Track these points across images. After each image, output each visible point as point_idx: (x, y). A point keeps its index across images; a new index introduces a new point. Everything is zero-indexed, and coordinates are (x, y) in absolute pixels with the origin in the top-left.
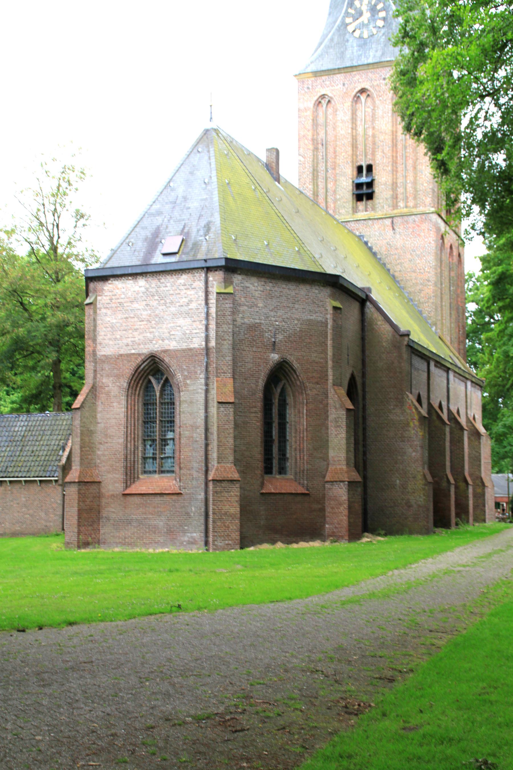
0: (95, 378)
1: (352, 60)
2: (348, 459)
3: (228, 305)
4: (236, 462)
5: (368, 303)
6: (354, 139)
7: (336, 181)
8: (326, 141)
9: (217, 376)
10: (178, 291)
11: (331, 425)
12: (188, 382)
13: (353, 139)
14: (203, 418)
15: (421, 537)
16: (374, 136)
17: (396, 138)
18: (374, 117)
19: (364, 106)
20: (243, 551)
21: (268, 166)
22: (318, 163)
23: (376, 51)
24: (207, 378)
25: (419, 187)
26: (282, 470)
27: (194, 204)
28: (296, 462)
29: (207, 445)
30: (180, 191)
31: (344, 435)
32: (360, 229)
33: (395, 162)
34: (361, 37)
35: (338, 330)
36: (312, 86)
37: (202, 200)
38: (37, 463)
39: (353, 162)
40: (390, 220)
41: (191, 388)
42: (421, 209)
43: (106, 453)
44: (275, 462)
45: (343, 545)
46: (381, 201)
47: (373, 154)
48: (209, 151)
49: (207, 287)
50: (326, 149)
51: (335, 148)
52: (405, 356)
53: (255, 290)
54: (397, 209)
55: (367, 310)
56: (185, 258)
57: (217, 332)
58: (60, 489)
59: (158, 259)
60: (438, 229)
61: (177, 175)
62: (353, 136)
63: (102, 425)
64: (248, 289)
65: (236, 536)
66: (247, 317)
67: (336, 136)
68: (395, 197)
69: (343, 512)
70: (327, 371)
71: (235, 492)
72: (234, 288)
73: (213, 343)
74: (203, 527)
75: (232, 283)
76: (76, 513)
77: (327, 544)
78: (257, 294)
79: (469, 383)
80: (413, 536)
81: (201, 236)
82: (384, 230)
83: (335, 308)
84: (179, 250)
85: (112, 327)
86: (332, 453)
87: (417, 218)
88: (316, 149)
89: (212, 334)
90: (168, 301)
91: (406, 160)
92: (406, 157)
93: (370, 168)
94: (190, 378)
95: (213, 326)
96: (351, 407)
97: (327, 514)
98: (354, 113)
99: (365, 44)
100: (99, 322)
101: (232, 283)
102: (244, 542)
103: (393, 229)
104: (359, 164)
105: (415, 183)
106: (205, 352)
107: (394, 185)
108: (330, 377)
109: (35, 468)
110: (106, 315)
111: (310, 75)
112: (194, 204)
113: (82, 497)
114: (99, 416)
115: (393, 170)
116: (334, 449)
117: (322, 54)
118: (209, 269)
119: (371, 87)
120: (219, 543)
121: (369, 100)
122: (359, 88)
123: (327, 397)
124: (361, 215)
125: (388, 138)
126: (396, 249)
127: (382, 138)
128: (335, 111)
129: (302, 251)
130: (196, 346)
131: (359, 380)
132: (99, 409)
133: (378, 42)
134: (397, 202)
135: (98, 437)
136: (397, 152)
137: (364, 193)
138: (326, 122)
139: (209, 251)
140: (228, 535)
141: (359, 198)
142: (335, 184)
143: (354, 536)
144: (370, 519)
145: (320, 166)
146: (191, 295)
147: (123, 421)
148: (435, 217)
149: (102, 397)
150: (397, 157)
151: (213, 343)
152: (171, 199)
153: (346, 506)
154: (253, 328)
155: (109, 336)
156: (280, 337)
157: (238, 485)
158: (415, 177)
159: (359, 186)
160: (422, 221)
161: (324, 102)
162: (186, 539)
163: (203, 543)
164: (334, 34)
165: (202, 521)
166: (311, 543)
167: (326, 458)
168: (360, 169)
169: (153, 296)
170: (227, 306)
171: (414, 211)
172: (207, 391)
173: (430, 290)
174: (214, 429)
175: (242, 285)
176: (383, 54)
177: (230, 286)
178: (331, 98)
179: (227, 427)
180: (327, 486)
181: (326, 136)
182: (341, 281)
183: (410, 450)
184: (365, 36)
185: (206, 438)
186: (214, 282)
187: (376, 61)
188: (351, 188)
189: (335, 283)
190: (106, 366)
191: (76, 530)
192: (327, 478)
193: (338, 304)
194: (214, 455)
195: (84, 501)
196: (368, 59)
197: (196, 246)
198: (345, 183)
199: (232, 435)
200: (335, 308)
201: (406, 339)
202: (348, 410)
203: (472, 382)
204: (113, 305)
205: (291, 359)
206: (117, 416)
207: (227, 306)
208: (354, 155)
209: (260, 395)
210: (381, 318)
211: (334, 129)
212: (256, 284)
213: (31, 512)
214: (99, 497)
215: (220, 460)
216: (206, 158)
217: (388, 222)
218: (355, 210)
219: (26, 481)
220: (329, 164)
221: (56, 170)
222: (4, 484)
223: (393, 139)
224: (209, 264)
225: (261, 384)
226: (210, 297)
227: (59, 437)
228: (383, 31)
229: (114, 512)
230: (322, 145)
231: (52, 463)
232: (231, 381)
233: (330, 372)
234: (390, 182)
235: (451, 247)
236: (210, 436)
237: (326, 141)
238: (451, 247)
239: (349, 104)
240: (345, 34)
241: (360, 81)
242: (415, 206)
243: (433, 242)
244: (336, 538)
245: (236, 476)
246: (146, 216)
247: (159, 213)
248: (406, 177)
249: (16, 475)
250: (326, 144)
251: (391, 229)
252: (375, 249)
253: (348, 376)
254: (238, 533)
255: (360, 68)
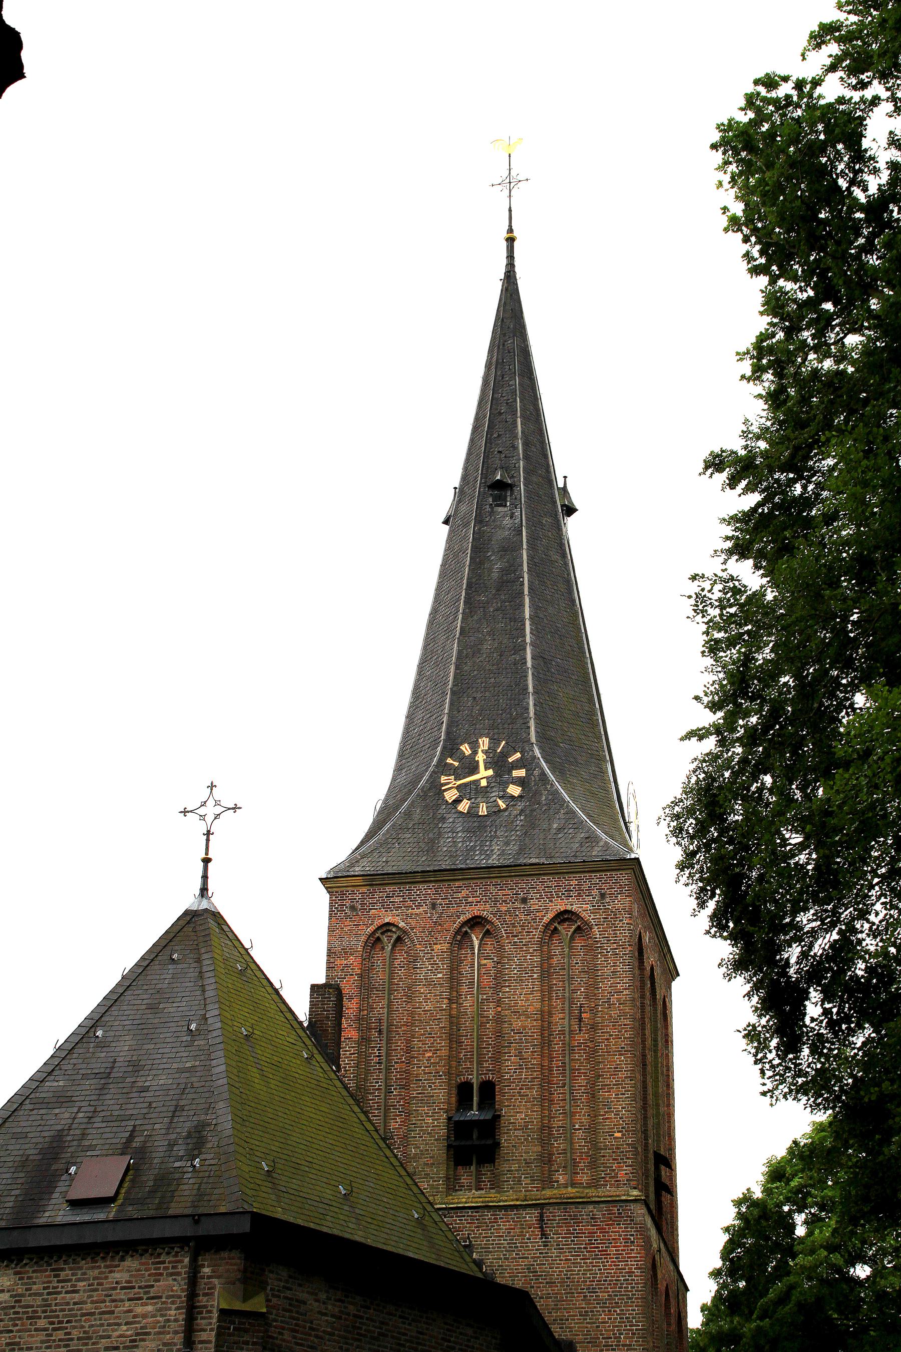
6: (454, 1021)
7: (409, 1114)
8: (390, 1025)
10: (108, 1305)
13: (451, 1023)
16: (499, 1020)
17: (549, 1028)
19: (478, 954)
23: (507, 844)
25: (603, 1140)
27: (159, 1080)
30: (124, 1049)
33: (546, 1081)
36: (363, 904)
37: (180, 1071)
39: (449, 1073)
40: (536, 1212)
42: (609, 1191)
46: (515, 1167)
47: (497, 1058)
48: (199, 961)
49: (192, 1295)
51: (408, 1041)
53: (320, 1312)
54: (552, 1187)
56: (132, 1211)
59: (57, 1212)
61: (114, 1011)
62: (451, 1016)
64: (303, 1308)
67: (412, 1014)
68: (546, 1159)
72: (268, 1300)
75: (262, 1285)
81: (181, 1159)
82: (522, 1235)
84: (117, 1193)
87: (598, 1212)
90: (75, 1333)
92: (573, 1070)
93: (488, 1090)
99: (482, 827)
101: (262, 1285)
103: (544, 1235)
105: (592, 1129)
107: (545, 1133)
111: (359, 881)
112: (159, 1080)
117: (386, 842)
119: (494, 915)
121: (489, 941)
122: (469, 916)
124: (465, 1198)
125: (532, 1025)
126: (551, 1283)
127: (518, 1024)
128: (413, 960)
129: (427, 1221)
133: (510, 826)
134: (551, 1172)
138: (391, 983)
139: (200, 1195)
146: (144, 1316)
150: (550, 1069)
152: (98, 1066)
158: (594, 1115)
161: (388, 942)
164: (412, 804)
168: (464, 1092)
169: (33, 1317)
175: (288, 1294)
176: (521, 851)
177: (257, 1293)
178: (405, 932)
184: (483, 810)
186: (216, 1281)
187: (507, 862)
196: (489, 857)
197: (166, 1181)
208: (453, 1058)
211: (410, 999)
212: (323, 1296)
216: (193, 974)
217: (531, 1216)
218: (452, 1185)
223: (542, 1029)
224: (207, 1228)
226: (201, 1322)
228: (520, 805)
230: (380, 1032)
234: (535, 1124)
237: (390, 1025)
240: (438, 806)
241: (472, 901)
242: (594, 1184)
243: (638, 1272)
246: (27, 1106)
247: (63, 1099)
250: (389, 1031)
251: (538, 1232)
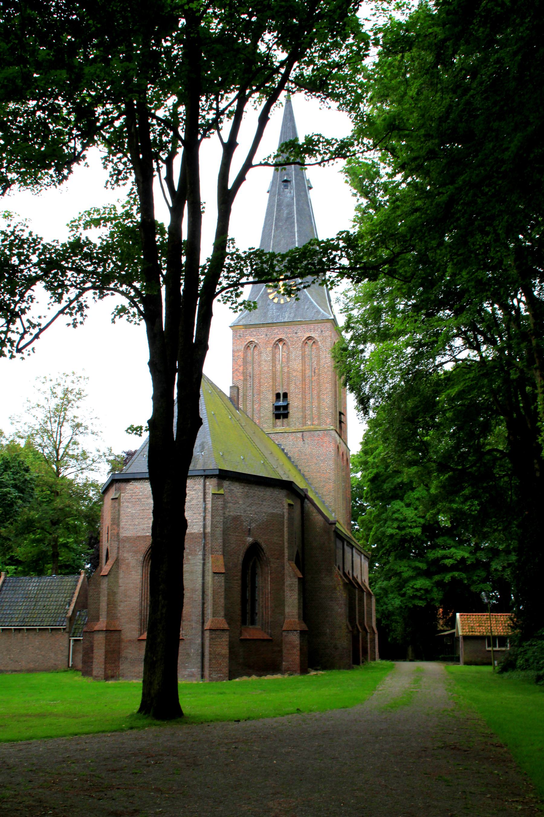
0: (118, 553)
1: (273, 318)
2: (299, 614)
3: (220, 502)
4: (226, 616)
5: (306, 500)
6: (274, 373)
9: (212, 554)
11: (287, 589)
12: (190, 557)
14: (201, 583)
15: (346, 671)
16: (288, 372)
18: (288, 360)
20: (231, 682)
21: (231, 399)
22: (247, 390)
23: (290, 313)
24: (204, 555)
26: (253, 623)
28: (263, 616)
29: (203, 604)
31: (296, 596)
32: (279, 439)
33: (304, 392)
34: (278, 303)
35: (291, 519)
38: (48, 615)
40: (301, 434)
41: (192, 562)
42: (324, 427)
43: (125, 609)
44: (248, 616)
45: (298, 677)
47: (288, 385)
49: (205, 490)
50: (253, 380)
51: (259, 380)
52: (333, 538)
55: (305, 505)
57: (212, 521)
58: (67, 635)
60: (336, 441)
63: (123, 588)
65: (226, 670)
66: (232, 511)
68: (304, 417)
69: (296, 652)
70: (284, 550)
71: (225, 639)
73: (208, 530)
74: (199, 665)
75: (222, 487)
76: (104, 654)
77: (286, 676)
78: (239, 495)
79: (363, 556)
80: (342, 670)
83: (290, 505)
85: (132, 516)
86: (287, 610)
87: (321, 433)
88: (245, 380)
89: (209, 523)
91: (312, 391)
93: (285, 395)
94: (191, 554)
95: (209, 517)
96: (301, 576)
97: (284, 654)
98: (274, 356)
99: (282, 308)
100: (122, 512)
101: (222, 487)
102: (231, 676)
104: (277, 392)
105: (319, 407)
106: (203, 536)
107: (304, 409)
108: (286, 554)
109: (47, 619)
110: (127, 507)
113: (108, 642)
114: (120, 581)
115: (303, 398)
116: (289, 606)
118: (206, 477)
120: (214, 676)
121: (285, 347)
123: (284, 569)
124: (279, 429)
125: (299, 375)
129: (266, 464)
130: (196, 531)
131: (300, 555)
132: (121, 575)
135: (119, 597)
136: (305, 385)
137: (281, 413)
139: (205, 463)
140: (220, 670)
141: (277, 416)
142: (259, 406)
143: (304, 671)
144: (315, 658)
145: (248, 392)
147: (139, 585)
148: (333, 432)
149: (123, 567)
151: (208, 530)
153: (298, 648)
154: (236, 519)
155: (129, 523)
156: (253, 525)
157: (227, 633)
158: (319, 403)
159: (277, 408)
160: (325, 436)
162: (187, 673)
163: (200, 676)
165: (199, 659)
166: (275, 676)
167: (283, 613)
168: (278, 396)
170: (220, 503)
171: (319, 428)
172: (204, 564)
173: (331, 486)
174: (209, 592)
176: (295, 316)
179: (219, 590)
180: (284, 634)
181: (253, 370)
182: (293, 486)
183: (337, 607)
185: (203, 598)
188: (272, 409)
189: (288, 487)
190: (127, 545)
191: (103, 667)
192: (284, 628)
193: (292, 503)
194: (209, 611)
195: (109, 645)
196: (284, 318)
198: (268, 405)
199: (223, 596)
200: (290, 505)
201: (334, 526)
202: (299, 578)
203: (364, 555)
204: (133, 500)
205: (260, 541)
206: (135, 582)
207: (220, 503)
208: (274, 385)
209: (240, 567)
210: (315, 511)
211: (259, 366)
213: (43, 653)
214: (120, 642)
215: (214, 614)
217: (299, 435)
218: (274, 425)
219: (39, 629)
220: (255, 391)
221: (59, 392)
222: (22, 631)
224: (207, 473)
225: (241, 558)
226: (207, 496)
227: (65, 595)
229: (131, 653)
231: (61, 615)
232: (222, 557)
233: (286, 551)
235: (343, 455)
236: (206, 597)
238: (343, 455)
239: (271, 349)
241: (278, 333)
242: (319, 424)
244: (96, 678)
245: (226, 626)
248: (312, 403)
249: (32, 624)
252: (289, 455)
253: (295, 553)
254: (227, 669)
255: (279, 324)
